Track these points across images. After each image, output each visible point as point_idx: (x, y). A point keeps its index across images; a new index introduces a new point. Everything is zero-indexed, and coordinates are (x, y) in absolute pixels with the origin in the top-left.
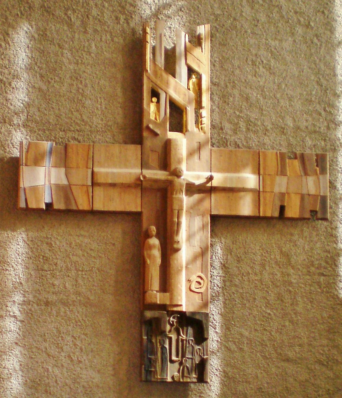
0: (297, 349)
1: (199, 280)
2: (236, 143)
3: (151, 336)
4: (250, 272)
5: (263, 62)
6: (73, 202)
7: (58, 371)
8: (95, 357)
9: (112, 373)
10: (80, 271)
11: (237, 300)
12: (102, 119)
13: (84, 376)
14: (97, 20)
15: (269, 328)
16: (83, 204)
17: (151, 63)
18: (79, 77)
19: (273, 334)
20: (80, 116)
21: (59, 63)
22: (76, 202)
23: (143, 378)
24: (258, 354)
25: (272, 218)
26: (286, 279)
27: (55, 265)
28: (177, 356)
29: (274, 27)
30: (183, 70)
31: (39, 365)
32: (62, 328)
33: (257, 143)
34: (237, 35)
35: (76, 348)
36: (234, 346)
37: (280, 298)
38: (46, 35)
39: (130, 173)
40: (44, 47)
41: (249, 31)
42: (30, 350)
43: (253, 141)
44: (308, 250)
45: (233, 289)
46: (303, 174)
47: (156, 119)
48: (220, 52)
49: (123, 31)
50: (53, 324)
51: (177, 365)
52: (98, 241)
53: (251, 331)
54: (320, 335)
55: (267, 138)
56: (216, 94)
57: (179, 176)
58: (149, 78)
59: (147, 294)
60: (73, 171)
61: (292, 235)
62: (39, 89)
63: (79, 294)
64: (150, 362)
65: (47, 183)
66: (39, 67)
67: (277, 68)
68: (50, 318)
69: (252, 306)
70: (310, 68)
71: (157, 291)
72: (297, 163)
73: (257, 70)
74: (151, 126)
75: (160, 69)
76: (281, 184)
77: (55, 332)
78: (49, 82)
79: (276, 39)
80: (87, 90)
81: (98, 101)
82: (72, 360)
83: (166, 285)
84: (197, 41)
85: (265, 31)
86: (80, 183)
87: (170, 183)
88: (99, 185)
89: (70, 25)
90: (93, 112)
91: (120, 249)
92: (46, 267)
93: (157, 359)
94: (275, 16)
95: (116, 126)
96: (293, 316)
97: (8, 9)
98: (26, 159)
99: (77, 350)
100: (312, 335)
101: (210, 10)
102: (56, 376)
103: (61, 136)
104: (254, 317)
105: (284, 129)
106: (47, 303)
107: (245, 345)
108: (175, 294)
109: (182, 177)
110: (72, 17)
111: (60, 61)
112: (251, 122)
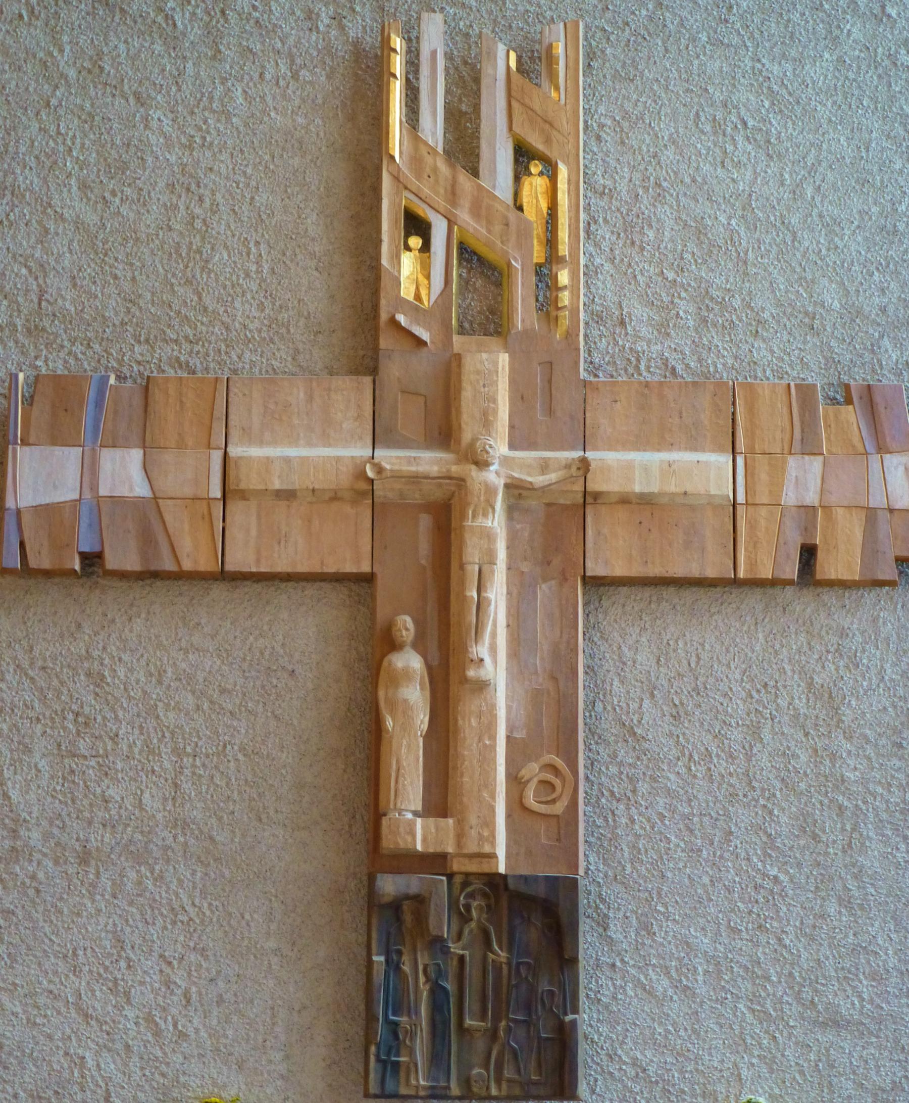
0: (866, 987)
1: (550, 777)
2: (666, 362)
5: (745, 124)
6: (165, 550)
7: (112, 1066)
8: (228, 1021)
9: (282, 1068)
10: (188, 755)
11: (673, 838)
12: (262, 303)
13: (194, 1082)
14: (252, 22)
15: (775, 924)
16: (194, 554)
17: (404, 132)
18: (193, 187)
20: (196, 298)
21: (137, 148)
23: (373, 1088)
25: (774, 583)
27: (111, 738)
29: (778, 23)
31: (58, 1048)
32: (128, 930)
33: (730, 361)
34: (667, 50)
35: (172, 993)
36: (666, 982)
37: (807, 827)
38: (101, 68)
39: (338, 459)
40: (92, 105)
42: (29, 1001)
43: (719, 355)
44: (892, 680)
46: (870, 448)
47: (418, 297)
48: (617, 99)
49: (328, 49)
50: (102, 920)
52: (245, 666)
53: (718, 933)
55: (763, 345)
56: (605, 220)
58: (396, 178)
59: (385, 821)
60: (169, 457)
62: (76, 222)
63: (180, 824)
64: (396, 1036)
65: (87, 495)
67: (790, 138)
68: (93, 901)
69: (721, 857)
70: (888, 137)
71: (416, 814)
73: (730, 148)
74: (401, 318)
75: (432, 151)
76: (804, 480)
77: (107, 943)
80: (219, 222)
81: (248, 254)
82: (157, 1034)
86: (188, 491)
87: (460, 482)
88: (243, 495)
89: (173, 40)
90: (233, 286)
91: (310, 685)
92: (83, 746)
95: (302, 322)
96: (852, 884)
99: (175, 998)
102: (107, 1080)
103: (140, 358)
107: (700, 978)
111: (140, 141)
112: (712, 299)
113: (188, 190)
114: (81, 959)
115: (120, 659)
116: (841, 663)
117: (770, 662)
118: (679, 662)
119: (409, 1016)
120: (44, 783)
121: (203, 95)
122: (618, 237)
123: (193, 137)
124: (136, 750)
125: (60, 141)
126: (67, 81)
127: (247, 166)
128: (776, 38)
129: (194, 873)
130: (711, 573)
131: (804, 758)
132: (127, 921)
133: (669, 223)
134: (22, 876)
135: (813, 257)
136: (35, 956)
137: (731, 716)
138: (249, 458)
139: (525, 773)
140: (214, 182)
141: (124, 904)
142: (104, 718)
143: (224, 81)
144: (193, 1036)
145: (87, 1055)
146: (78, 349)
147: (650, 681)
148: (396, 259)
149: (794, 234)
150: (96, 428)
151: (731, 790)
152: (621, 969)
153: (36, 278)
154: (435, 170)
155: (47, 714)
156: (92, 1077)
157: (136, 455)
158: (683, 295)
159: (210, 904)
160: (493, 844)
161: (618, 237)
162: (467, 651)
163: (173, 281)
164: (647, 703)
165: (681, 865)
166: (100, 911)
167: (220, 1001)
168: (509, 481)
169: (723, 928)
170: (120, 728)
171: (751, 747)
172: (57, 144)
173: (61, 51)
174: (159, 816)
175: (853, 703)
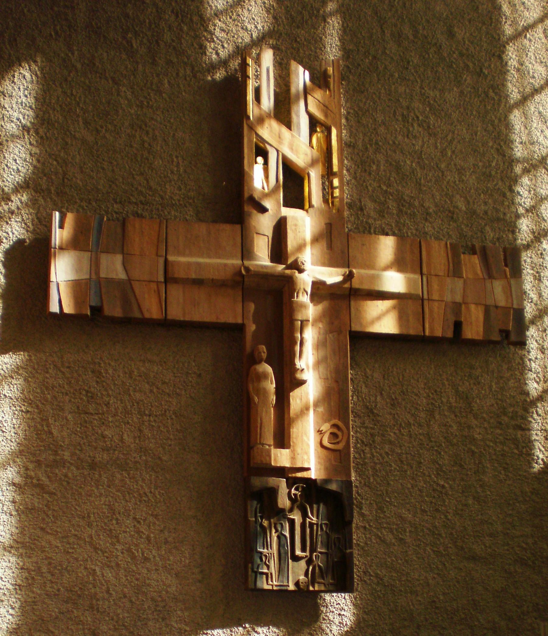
1: (335, 431)
5: (418, 117)
7: (110, 575)
10: (146, 415)
13: (153, 583)
15: (443, 508)
16: (152, 311)
18: (144, 126)
27: (106, 405)
28: (303, 550)
29: (432, 72)
31: (81, 565)
33: (414, 232)
34: (379, 80)
35: (141, 537)
36: (391, 536)
38: (94, 64)
39: (226, 265)
40: (90, 82)
41: (396, 75)
43: (408, 228)
45: (387, 447)
46: (486, 277)
51: (303, 563)
61: (472, 367)
65: (94, 277)
70: (485, 130)
73: (411, 129)
79: (435, 87)
80: (157, 146)
82: (134, 557)
83: (283, 440)
88: (176, 281)
90: (165, 177)
92: (91, 408)
95: (201, 197)
102: (107, 582)
105: (453, 213)
112: (404, 201)
113: (141, 128)
114: (92, 518)
115: (109, 364)
116: (472, 382)
117: (437, 380)
118: (394, 378)
119: (267, 549)
120: (71, 427)
121: (147, 81)
122: (358, 167)
123: (142, 101)
124: (119, 412)
125: (73, 98)
126: (76, 69)
127: (171, 118)
128: (431, 79)
129: (151, 476)
131: (455, 428)
132: (116, 500)
133: (382, 162)
134: (59, 474)
135: (452, 184)
136: (67, 517)
137: (420, 406)
138: (179, 263)
140: (154, 125)
141: (114, 491)
142: (102, 394)
143: (158, 75)
144: (152, 559)
145: (97, 568)
147: (380, 387)
148: (251, 167)
149: (443, 172)
151: (420, 442)
152: (369, 530)
153: (61, 167)
155: (72, 391)
156: (99, 580)
157: (118, 259)
158: (391, 197)
159: (159, 492)
160: (309, 461)
161: (358, 167)
162: (295, 365)
163: (134, 172)
164: (379, 398)
165: (397, 478)
166: (101, 494)
167: (166, 542)
168: (314, 280)
169: (418, 510)
170: (110, 400)
171: (430, 421)
172: (71, 99)
173: (73, 54)
174: (132, 446)
175: (478, 401)
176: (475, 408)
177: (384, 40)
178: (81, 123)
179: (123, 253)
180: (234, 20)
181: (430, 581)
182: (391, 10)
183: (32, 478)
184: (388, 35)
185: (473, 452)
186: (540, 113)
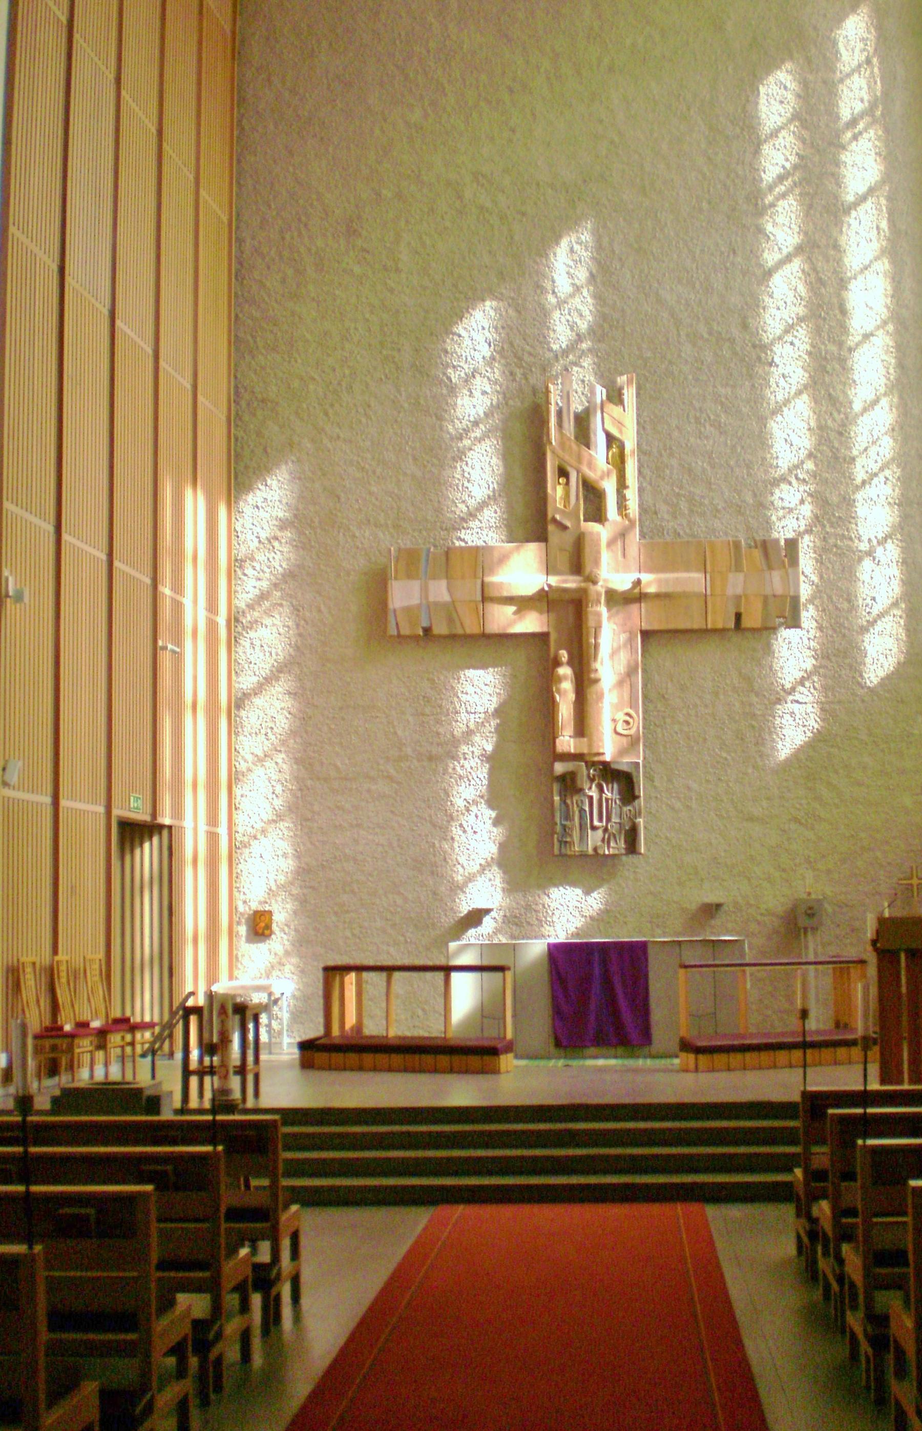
0: (765, 803)
1: (628, 718)
2: (675, 531)
3: (565, 796)
4: (699, 703)
5: (709, 418)
6: (458, 624)
16: (471, 627)
19: (731, 785)
22: (462, 624)
23: (556, 852)
24: (711, 813)
25: (723, 631)
26: (747, 710)
28: (600, 820)
30: (600, 440)
33: (704, 529)
38: (419, 403)
41: (690, 377)
43: (699, 526)
45: (676, 727)
46: (765, 568)
49: (521, 390)
51: (600, 833)
54: (796, 783)
57: (595, 583)
58: (553, 452)
59: (557, 741)
61: (754, 650)
66: (411, 447)
67: (730, 424)
72: (757, 554)
73: (703, 429)
74: (558, 517)
75: (569, 439)
76: (736, 584)
78: (425, 466)
79: (727, 384)
83: (582, 727)
84: (615, 396)
85: (713, 376)
87: (584, 591)
92: (427, 711)
93: (574, 825)
94: (726, 352)
96: (758, 759)
97: (369, 371)
98: (396, 571)
100: (785, 784)
101: (637, 353)
104: (706, 764)
105: (740, 507)
106: (431, 758)
108: (595, 738)
109: (600, 584)
110: (452, 377)
130: (695, 626)
139: (617, 717)
146: (416, 534)
148: (555, 489)
150: (426, 572)
154: (570, 447)
157: (443, 583)
173: (401, 395)
176: (756, 688)
177: (679, 342)
178: (411, 460)
179: (447, 578)
180: (541, 343)
181: (713, 841)
182: (687, 310)
183: (382, 771)
184: (683, 337)
185: (753, 727)
186: (830, 395)
